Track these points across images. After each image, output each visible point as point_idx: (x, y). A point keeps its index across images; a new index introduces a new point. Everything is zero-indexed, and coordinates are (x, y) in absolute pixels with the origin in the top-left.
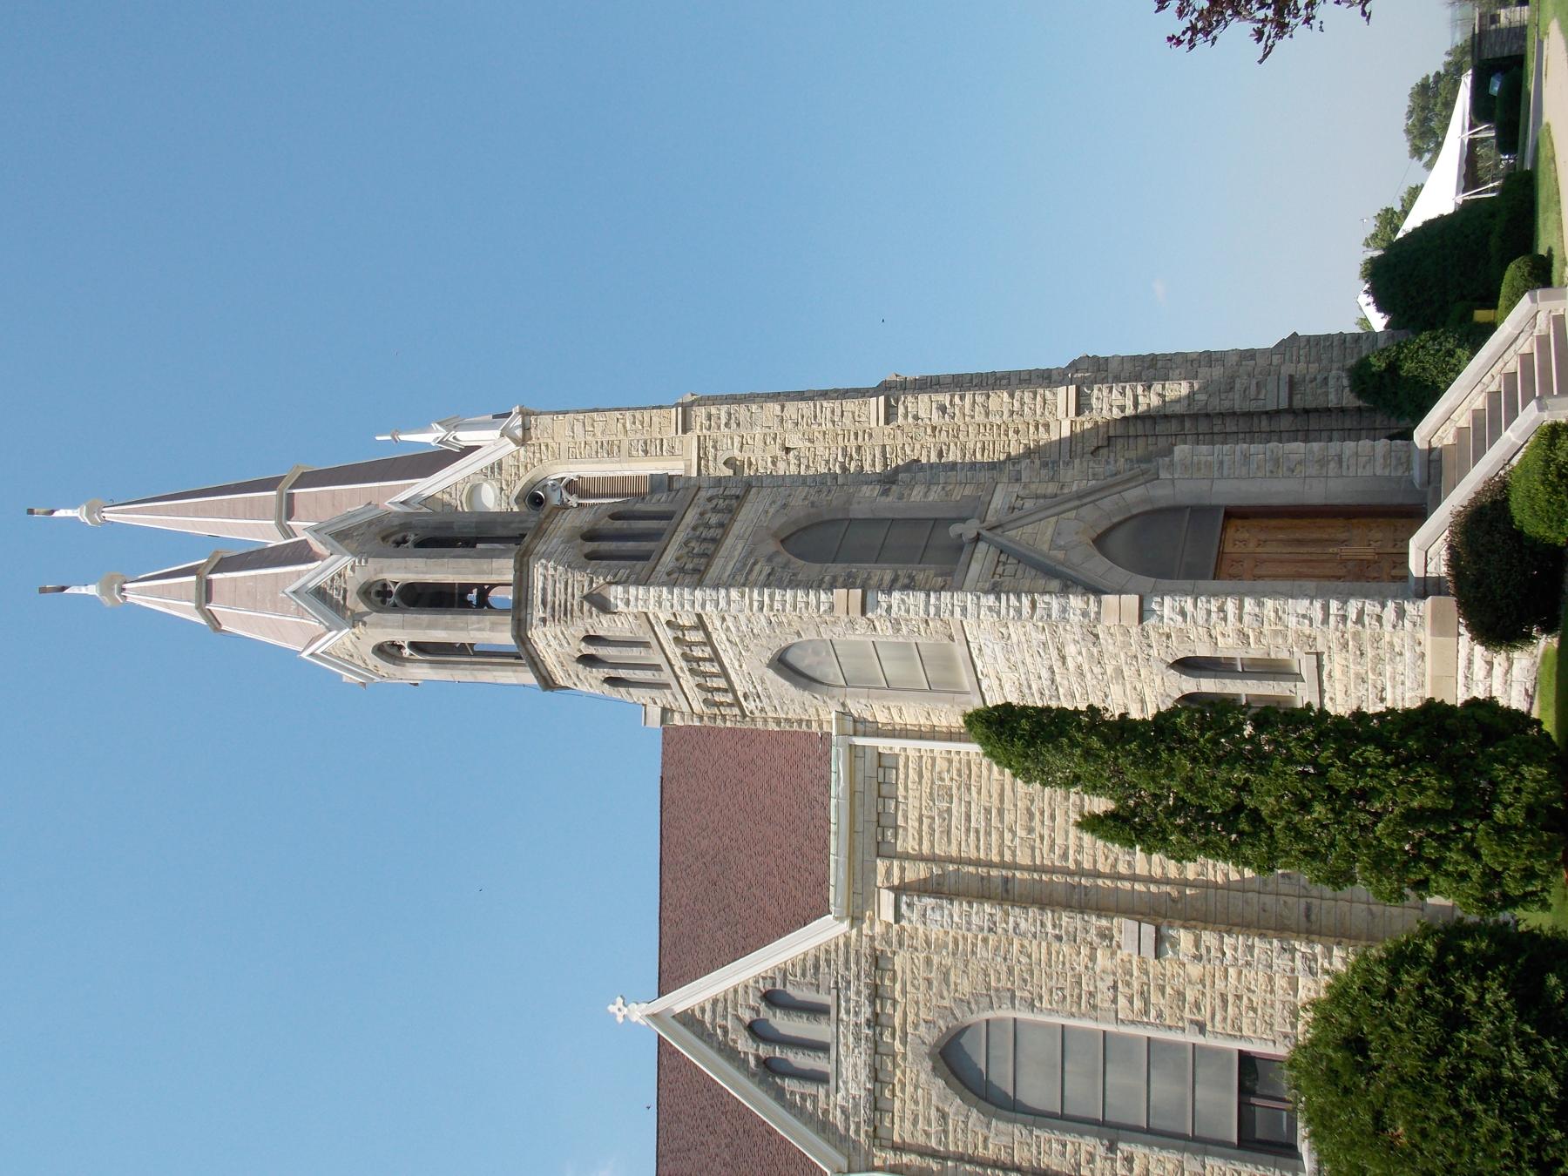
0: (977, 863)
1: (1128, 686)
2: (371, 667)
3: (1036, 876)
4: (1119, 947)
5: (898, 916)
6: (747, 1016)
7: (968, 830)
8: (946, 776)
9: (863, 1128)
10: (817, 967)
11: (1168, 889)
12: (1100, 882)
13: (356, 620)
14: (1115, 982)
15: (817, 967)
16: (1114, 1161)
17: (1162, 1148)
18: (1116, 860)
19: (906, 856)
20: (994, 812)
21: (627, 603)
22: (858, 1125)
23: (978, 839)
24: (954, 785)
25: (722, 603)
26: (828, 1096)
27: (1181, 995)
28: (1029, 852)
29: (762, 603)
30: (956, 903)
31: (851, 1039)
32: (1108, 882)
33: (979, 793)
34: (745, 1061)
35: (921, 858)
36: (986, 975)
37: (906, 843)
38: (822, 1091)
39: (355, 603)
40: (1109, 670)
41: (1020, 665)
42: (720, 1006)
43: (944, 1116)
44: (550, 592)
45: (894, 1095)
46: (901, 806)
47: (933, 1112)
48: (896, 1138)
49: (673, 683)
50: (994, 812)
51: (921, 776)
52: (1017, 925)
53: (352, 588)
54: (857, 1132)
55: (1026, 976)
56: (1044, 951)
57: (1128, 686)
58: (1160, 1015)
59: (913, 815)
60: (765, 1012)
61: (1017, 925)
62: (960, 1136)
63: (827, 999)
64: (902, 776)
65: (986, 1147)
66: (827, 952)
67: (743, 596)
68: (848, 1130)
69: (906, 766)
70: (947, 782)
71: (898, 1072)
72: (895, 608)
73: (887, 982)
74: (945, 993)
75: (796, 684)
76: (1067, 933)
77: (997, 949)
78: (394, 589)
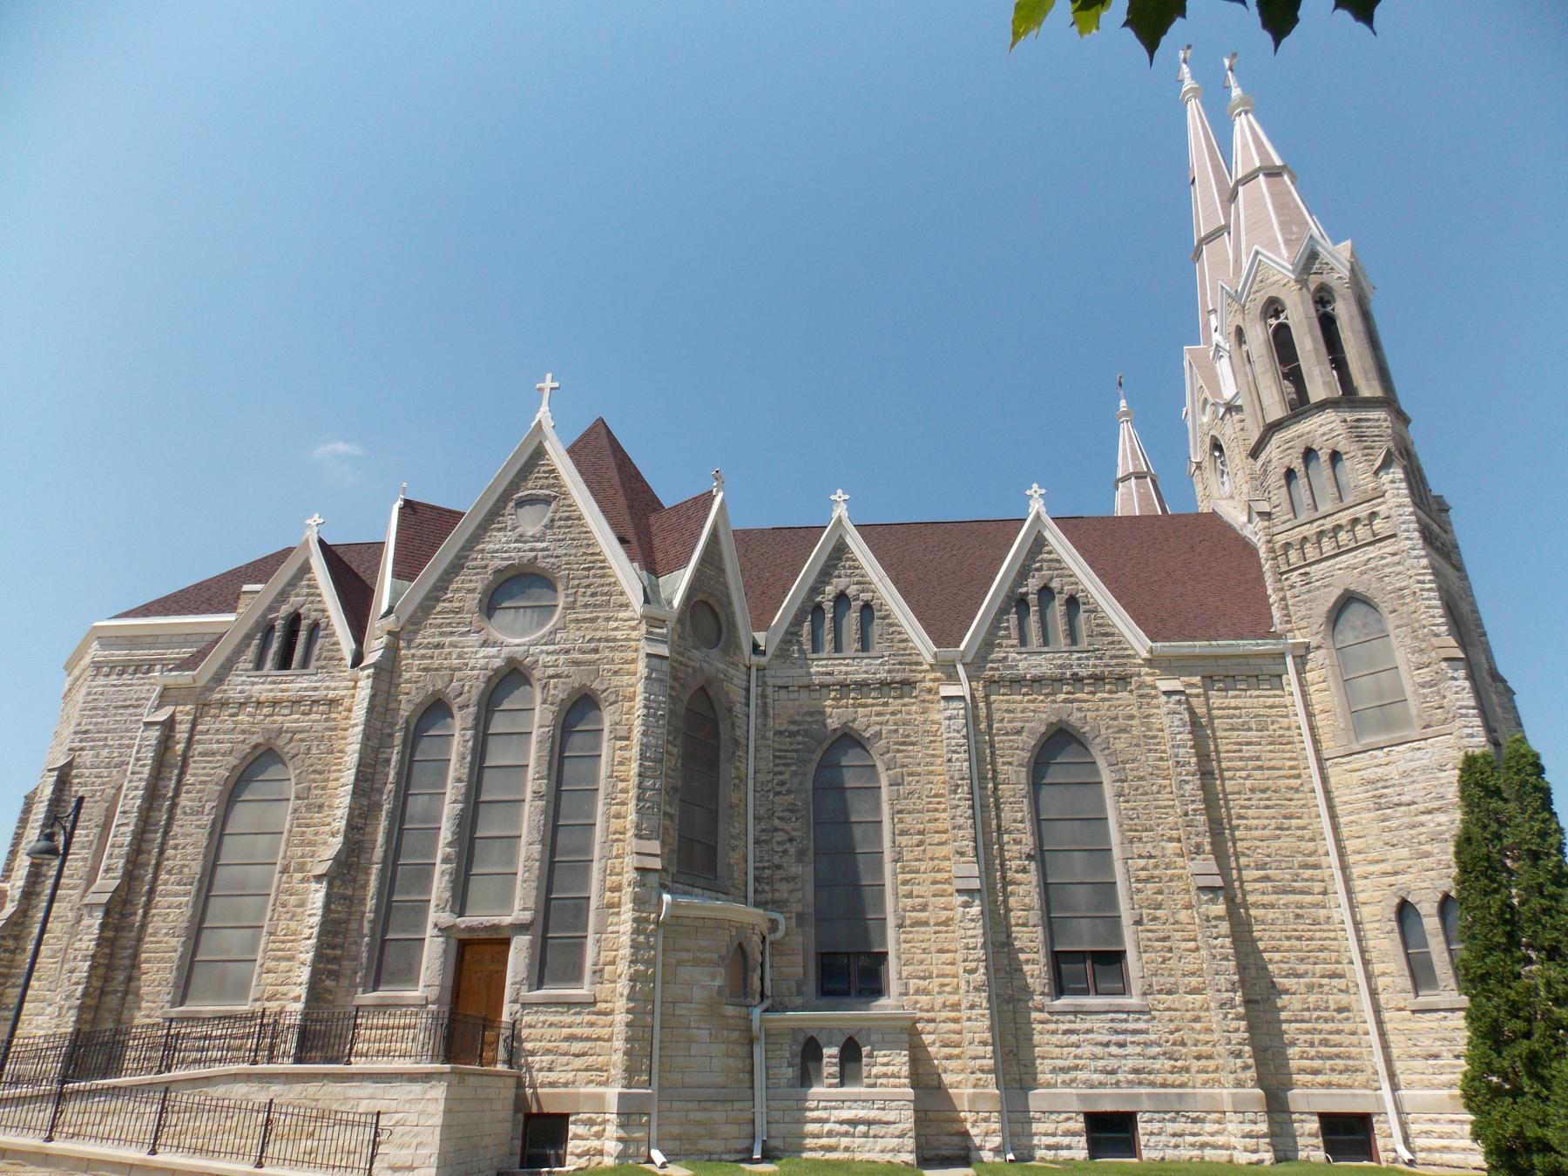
0: (1217, 752)
1: (1410, 862)
2: (1251, 297)
3: (1221, 796)
4: (1193, 859)
5: (1168, 693)
6: (1055, 584)
7: (1239, 744)
8: (1276, 726)
9: (997, 674)
10: (1106, 634)
11: (1240, 896)
12: (1230, 844)
13: (1302, 282)
14: (1155, 857)
15: (1106, 634)
16: (1020, 859)
17: (1039, 894)
18: (1248, 856)
19: (1207, 699)
20: (1259, 763)
21: (1392, 482)
22: (997, 669)
23: (1235, 752)
24: (1271, 733)
25: (1415, 553)
26: (1012, 646)
27: (1159, 906)
28: (1236, 790)
29: (1423, 582)
30: (1190, 736)
31: (1059, 662)
32: (1231, 850)
33: (1270, 751)
34: (1021, 585)
35: (1210, 709)
36: (1134, 761)
37: (1216, 699)
38: (1016, 642)
39: (1313, 284)
40: (1427, 847)
41: (1410, 779)
42: (1057, 565)
43: (1019, 732)
44: (1369, 424)
45: (1024, 695)
46: (1243, 693)
47: (1019, 725)
48: (993, 698)
49: (1296, 522)
50: (1259, 763)
51: (1271, 707)
52: (1187, 782)
53: (1325, 278)
54: (992, 669)
55: (1140, 791)
56: (1166, 803)
57: (1410, 862)
58: (1139, 891)
59: (1239, 702)
60: (856, 605)
61: (1187, 782)
62: (1007, 744)
63: (1084, 643)
64: (1267, 693)
65: (1004, 764)
66: (1120, 642)
67: (1424, 568)
68: (992, 662)
69: (1275, 696)
70: (1271, 727)
71: (1042, 697)
72: (1457, 683)
73: (1107, 687)
74: (1110, 731)
75: (1330, 611)
76: (1192, 820)
77: (1158, 768)
78: (1329, 309)
